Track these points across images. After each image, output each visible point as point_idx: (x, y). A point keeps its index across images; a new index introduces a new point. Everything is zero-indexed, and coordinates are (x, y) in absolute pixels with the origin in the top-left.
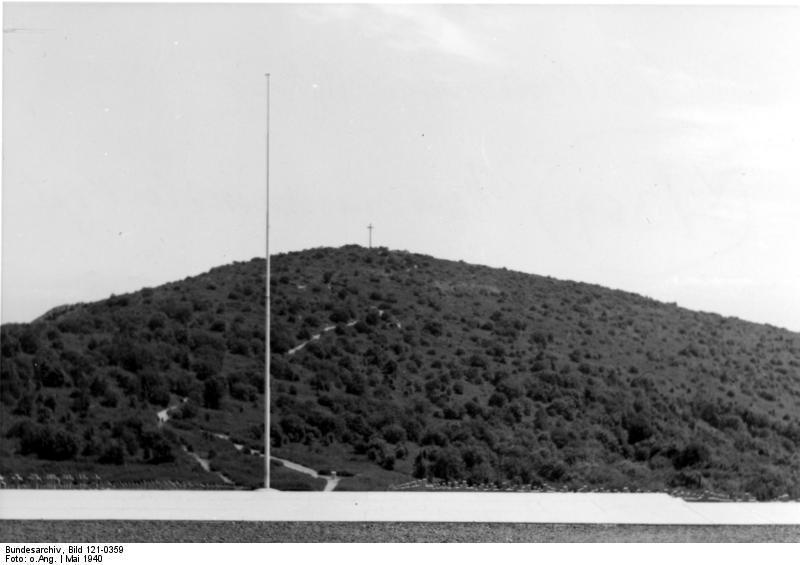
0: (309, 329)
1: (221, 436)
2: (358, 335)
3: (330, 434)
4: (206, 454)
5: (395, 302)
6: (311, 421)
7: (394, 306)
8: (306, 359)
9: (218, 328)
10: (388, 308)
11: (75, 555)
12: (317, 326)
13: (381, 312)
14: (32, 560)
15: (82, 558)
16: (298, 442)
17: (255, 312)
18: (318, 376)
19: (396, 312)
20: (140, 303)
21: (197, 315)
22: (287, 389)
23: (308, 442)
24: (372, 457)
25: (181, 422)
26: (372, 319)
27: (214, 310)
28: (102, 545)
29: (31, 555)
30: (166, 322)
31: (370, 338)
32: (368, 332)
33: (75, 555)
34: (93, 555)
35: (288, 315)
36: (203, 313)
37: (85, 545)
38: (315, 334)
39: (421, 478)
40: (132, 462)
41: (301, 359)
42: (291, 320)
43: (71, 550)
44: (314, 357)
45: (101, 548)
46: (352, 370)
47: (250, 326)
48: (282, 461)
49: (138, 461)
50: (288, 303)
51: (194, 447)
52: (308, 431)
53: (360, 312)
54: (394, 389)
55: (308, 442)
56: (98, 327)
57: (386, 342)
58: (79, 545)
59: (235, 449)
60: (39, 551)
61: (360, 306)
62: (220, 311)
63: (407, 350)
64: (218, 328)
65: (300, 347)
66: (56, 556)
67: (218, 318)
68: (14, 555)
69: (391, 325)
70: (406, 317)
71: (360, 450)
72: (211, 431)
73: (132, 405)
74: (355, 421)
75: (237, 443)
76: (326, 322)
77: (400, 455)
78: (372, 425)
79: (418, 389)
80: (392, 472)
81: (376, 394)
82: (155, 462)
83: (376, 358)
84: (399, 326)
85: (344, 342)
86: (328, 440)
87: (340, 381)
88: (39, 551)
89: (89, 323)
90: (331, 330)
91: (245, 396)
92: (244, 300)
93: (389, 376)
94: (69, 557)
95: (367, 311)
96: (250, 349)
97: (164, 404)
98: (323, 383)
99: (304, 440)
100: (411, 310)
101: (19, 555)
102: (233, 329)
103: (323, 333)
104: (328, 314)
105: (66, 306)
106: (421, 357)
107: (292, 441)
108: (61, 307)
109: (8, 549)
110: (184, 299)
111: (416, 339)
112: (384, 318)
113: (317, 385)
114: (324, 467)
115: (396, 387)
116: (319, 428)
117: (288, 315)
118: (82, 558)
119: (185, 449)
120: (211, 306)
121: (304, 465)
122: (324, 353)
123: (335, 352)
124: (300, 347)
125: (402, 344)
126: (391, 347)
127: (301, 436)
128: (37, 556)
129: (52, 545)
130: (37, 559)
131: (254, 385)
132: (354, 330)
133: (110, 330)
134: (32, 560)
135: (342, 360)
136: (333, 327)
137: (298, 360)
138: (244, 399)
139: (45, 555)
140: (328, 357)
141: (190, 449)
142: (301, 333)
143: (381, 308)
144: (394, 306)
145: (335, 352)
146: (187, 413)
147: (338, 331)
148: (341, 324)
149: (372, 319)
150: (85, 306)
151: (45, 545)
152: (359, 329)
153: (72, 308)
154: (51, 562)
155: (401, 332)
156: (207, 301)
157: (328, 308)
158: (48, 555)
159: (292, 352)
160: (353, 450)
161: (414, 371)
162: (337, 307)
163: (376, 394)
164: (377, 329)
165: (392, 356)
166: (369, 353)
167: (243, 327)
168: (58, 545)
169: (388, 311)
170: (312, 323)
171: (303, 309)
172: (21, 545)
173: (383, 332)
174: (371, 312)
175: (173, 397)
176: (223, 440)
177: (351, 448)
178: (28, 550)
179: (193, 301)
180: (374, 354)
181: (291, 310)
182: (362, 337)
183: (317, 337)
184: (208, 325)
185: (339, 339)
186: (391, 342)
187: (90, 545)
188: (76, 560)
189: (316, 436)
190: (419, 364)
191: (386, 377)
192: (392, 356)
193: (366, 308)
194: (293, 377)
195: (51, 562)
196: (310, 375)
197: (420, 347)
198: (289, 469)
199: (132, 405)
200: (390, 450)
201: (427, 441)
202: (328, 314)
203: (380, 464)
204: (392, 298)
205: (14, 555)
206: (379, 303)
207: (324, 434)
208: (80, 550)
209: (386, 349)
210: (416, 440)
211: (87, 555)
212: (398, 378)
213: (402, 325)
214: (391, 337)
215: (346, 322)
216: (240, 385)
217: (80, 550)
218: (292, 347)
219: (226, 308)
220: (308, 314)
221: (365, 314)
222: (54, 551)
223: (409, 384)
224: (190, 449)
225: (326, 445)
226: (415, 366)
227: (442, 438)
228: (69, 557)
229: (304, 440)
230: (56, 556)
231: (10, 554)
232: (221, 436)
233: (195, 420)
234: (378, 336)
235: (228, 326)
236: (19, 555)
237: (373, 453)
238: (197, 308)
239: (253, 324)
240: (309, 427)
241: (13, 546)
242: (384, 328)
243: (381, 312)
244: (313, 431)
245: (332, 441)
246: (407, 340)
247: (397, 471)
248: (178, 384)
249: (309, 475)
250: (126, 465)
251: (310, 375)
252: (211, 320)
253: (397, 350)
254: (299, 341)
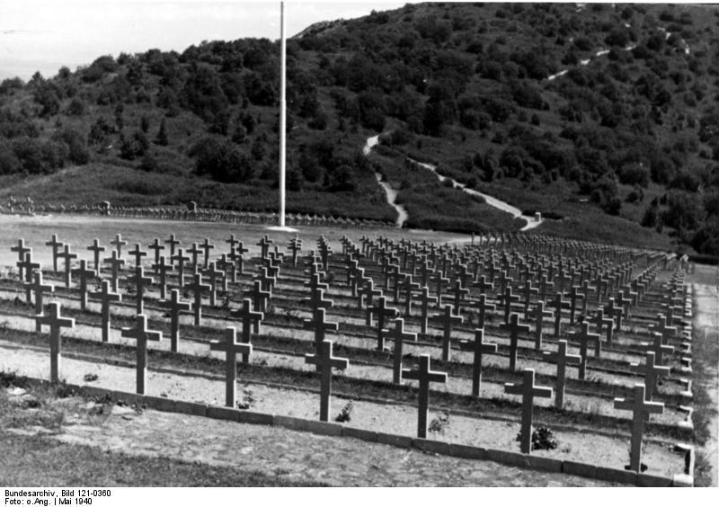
0: (577, 53)
1: (426, 166)
2: (635, 61)
3: (556, 170)
4: (398, 185)
5: (690, 23)
6: (536, 155)
7: (685, 28)
8: (564, 86)
9: (474, 49)
10: (679, 30)
11: (68, 498)
12: (588, 50)
13: (668, 35)
14: (29, 502)
15: (74, 501)
16: (515, 176)
17: (521, 32)
18: (570, 105)
19: (686, 35)
20: (401, 20)
21: (455, 35)
22: (530, 119)
23: (526, 178)
24: (596, 199)
25: (389, 149)
26: (655, 43)
27: (476, 29)
28: (91, 489)
29: (28, 498)
30: (416, 42)
31: (648, 65)
32: (647, 57)
33: (68, 498)
34: (84, 498)
35: (558, 35)
36: (464, 33)
37: (76, 489)
38: (585, 59)
39: (650, 226)
40: (309, 189)
41: (558, 85)
42: (560, 42)
43: (63, 493)
44: (575, 85)
45: (91, 492)
46: (614, 100)
47: (512, 47)
48: (484, 196)
49: (318, 189)
50: (561, 22)
51: (388, 178)
52: (527, 164)
53: (643, 34)
54: (660, 123)
55: (526, 178)
56: (343, 46)
57: (666, 69)
58: (71, 489)
59: (438, 179)
60: (35, 494)
61: (644, 27)
62: (482, 31)
63: (689, 80)
64: (474, 49)
65: (562, 73)
66: (51, 499)
67: (475, 39)
68: (13, 498)
69: (677, 51)
70: (697, 41)
71: (585, 190)
72: (414, 158)
73: (341, 128)
74: (592, 157)
75: (442, 174)
76: (599, 45)
77: (632, 198)
78: (611, 163)
79: (691, 125)
80: (616, 219)
81: (633, 128)
82: (333, 190)
83: (647, 88)
84: (687, 51)
85: (615, 68)
86: (551, 177)
87: (596, 111)
88: (35, 494)
89: (333, 41)
90: (605, 55)
91: (474, 123)
92: (511, 19)
93: (659, 109)
94: (63, 500)
95: (651, 33)
96: (502, 73)
97: (378, 128)
98: (575, 113)
99: (522, 175)
100: (706, 33)
101: (17, 498)
102: (491, 50)
103: (592, 58)
104: (603, 36)
105: (325, 23)
106: (706, 88)
107: (507, 175)
108: (320, 24)
109: (7, 493)
110: (446, 17)
111: (704, 68)
112: (671, 42)
113: (566, 115)
114: (530, 207)
115: (664, 120)
116: (543, 162)
117: (558, 35)
118: (74, 501)
119: (379, 178)
120: (474, 25)
121: (510, 203)
122: (587, 81)
123: (601, 79)
124: (562, 73)
125: (687, 72)
126: (671, 76)
127: (519, 169)
128: (33, 499)
129: (47, 489)
130: (33, 501)
131: (490, 112)
132: (631, 55)
133: (356, 48)
134: (29, 502)
135: (605, 89)
136: (607, 52)
137: (554, 87)
138: (473, 128)
139: (40, 498)
140: (591, 85)
141: (384, 179)
142: (566, 57)
143: (668, 30)
144: (685, 28)
145: (601, 79)
146: (398, 139)
147: (612, 56)
148: (616, 47)
149: (655, 43)
150: (345, 23)
151: (41, 489)
152: (637, 54)
153: (332, 25)
154: (46, 505)
155: (688, 58)
156: (470, 20)
157: (605, 28)
158: (43, 498)
159: (552, 77)
160: (579, 190)
161: (692, 104)
162: (617, 28)
163: (633, 128)
164: (660, 56)
165: (669, 85)
166: (641, 81)
167: (502, 49)
168: (52, 489)
169: (677, 33)
170: (582, 46)
171: (577, 30)
172: (18, 490)
173: (665, 58)
174: (655, 35)
175: (389, 120)
176: (428, 170)
177: (577, 188)
178: (25, 494)
179: (455, 19)
180: (646, 83)
181: (562, 32)
182: (640, 63)
183: (585, 62)
184: (464, 45)
185: (610, 65)
186: (672, 69)
187: (81, 489)
188: (67, 502)
189: (537, 171)
190: (699, 97)
191: (654, 109)
192: (669, 85)
193: (651, 29)
194: (543, 105)
195: (46, 505)
196: (564, 103)
197: (707, 75)
198: (491, 206)
199: (341, 128)
200: (623, 190)
201: (676, 184)
202: (603, 36)
203: (603, 207)
204: (686, 19)
205: (13, 498)
206: (669, 24)
207: (548, 168)
208: (72, 494)
209: (663, 78)
210: (666, 182)
211: (79, 498)
212: (670, 110)
213: (691, 51)
214: (673, 64)
215: (623, 45)
216: (470, 112)
217: (72, 494)
218: (553, 72)
219: (489, 27)
220: (580, 35)
221: (648, 36)
222: (48, 495)
223: (681, 118)
224: (384, 179)
225: (548, 182)
226: (694, 98)
227: (695, 182)
228: (63, 500)
229: (522, 175)
230: (51, 499)
231: (9, 497)
232: (426, 166)
233: (405, 148)
234: (657, 62)
235: (486, 47)
236: (17, 498)
237: (597, 194)
238: (457, 27)
239: (515, 46)
240: (532, 160)
241: (11, 490)
242: (668, 53)
243: (668, 35)
244: (535, 167)
245: (555, 179)
246: (693, 67)
247: (623, 216)
248: (401, 107)
249: (510, 215)
250: (302, 191)
251: (564, 103)
252: (468, 41)
253: (677, 78)
254: (564, 66)
